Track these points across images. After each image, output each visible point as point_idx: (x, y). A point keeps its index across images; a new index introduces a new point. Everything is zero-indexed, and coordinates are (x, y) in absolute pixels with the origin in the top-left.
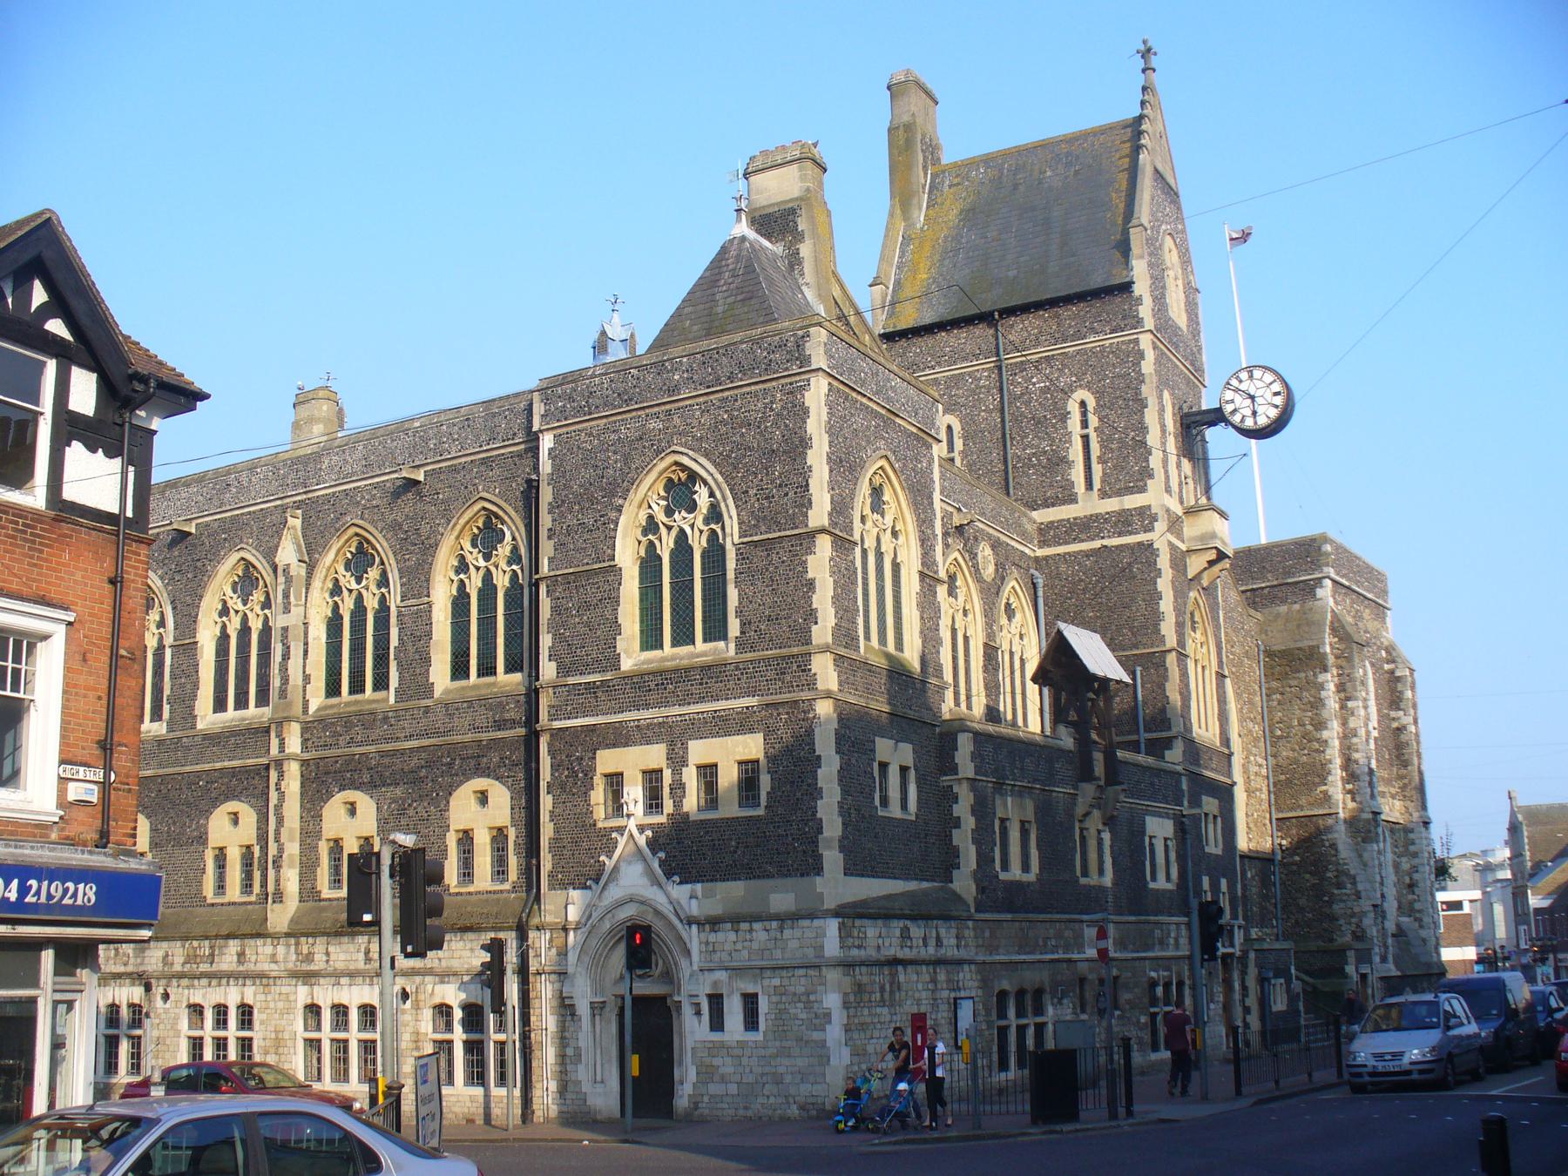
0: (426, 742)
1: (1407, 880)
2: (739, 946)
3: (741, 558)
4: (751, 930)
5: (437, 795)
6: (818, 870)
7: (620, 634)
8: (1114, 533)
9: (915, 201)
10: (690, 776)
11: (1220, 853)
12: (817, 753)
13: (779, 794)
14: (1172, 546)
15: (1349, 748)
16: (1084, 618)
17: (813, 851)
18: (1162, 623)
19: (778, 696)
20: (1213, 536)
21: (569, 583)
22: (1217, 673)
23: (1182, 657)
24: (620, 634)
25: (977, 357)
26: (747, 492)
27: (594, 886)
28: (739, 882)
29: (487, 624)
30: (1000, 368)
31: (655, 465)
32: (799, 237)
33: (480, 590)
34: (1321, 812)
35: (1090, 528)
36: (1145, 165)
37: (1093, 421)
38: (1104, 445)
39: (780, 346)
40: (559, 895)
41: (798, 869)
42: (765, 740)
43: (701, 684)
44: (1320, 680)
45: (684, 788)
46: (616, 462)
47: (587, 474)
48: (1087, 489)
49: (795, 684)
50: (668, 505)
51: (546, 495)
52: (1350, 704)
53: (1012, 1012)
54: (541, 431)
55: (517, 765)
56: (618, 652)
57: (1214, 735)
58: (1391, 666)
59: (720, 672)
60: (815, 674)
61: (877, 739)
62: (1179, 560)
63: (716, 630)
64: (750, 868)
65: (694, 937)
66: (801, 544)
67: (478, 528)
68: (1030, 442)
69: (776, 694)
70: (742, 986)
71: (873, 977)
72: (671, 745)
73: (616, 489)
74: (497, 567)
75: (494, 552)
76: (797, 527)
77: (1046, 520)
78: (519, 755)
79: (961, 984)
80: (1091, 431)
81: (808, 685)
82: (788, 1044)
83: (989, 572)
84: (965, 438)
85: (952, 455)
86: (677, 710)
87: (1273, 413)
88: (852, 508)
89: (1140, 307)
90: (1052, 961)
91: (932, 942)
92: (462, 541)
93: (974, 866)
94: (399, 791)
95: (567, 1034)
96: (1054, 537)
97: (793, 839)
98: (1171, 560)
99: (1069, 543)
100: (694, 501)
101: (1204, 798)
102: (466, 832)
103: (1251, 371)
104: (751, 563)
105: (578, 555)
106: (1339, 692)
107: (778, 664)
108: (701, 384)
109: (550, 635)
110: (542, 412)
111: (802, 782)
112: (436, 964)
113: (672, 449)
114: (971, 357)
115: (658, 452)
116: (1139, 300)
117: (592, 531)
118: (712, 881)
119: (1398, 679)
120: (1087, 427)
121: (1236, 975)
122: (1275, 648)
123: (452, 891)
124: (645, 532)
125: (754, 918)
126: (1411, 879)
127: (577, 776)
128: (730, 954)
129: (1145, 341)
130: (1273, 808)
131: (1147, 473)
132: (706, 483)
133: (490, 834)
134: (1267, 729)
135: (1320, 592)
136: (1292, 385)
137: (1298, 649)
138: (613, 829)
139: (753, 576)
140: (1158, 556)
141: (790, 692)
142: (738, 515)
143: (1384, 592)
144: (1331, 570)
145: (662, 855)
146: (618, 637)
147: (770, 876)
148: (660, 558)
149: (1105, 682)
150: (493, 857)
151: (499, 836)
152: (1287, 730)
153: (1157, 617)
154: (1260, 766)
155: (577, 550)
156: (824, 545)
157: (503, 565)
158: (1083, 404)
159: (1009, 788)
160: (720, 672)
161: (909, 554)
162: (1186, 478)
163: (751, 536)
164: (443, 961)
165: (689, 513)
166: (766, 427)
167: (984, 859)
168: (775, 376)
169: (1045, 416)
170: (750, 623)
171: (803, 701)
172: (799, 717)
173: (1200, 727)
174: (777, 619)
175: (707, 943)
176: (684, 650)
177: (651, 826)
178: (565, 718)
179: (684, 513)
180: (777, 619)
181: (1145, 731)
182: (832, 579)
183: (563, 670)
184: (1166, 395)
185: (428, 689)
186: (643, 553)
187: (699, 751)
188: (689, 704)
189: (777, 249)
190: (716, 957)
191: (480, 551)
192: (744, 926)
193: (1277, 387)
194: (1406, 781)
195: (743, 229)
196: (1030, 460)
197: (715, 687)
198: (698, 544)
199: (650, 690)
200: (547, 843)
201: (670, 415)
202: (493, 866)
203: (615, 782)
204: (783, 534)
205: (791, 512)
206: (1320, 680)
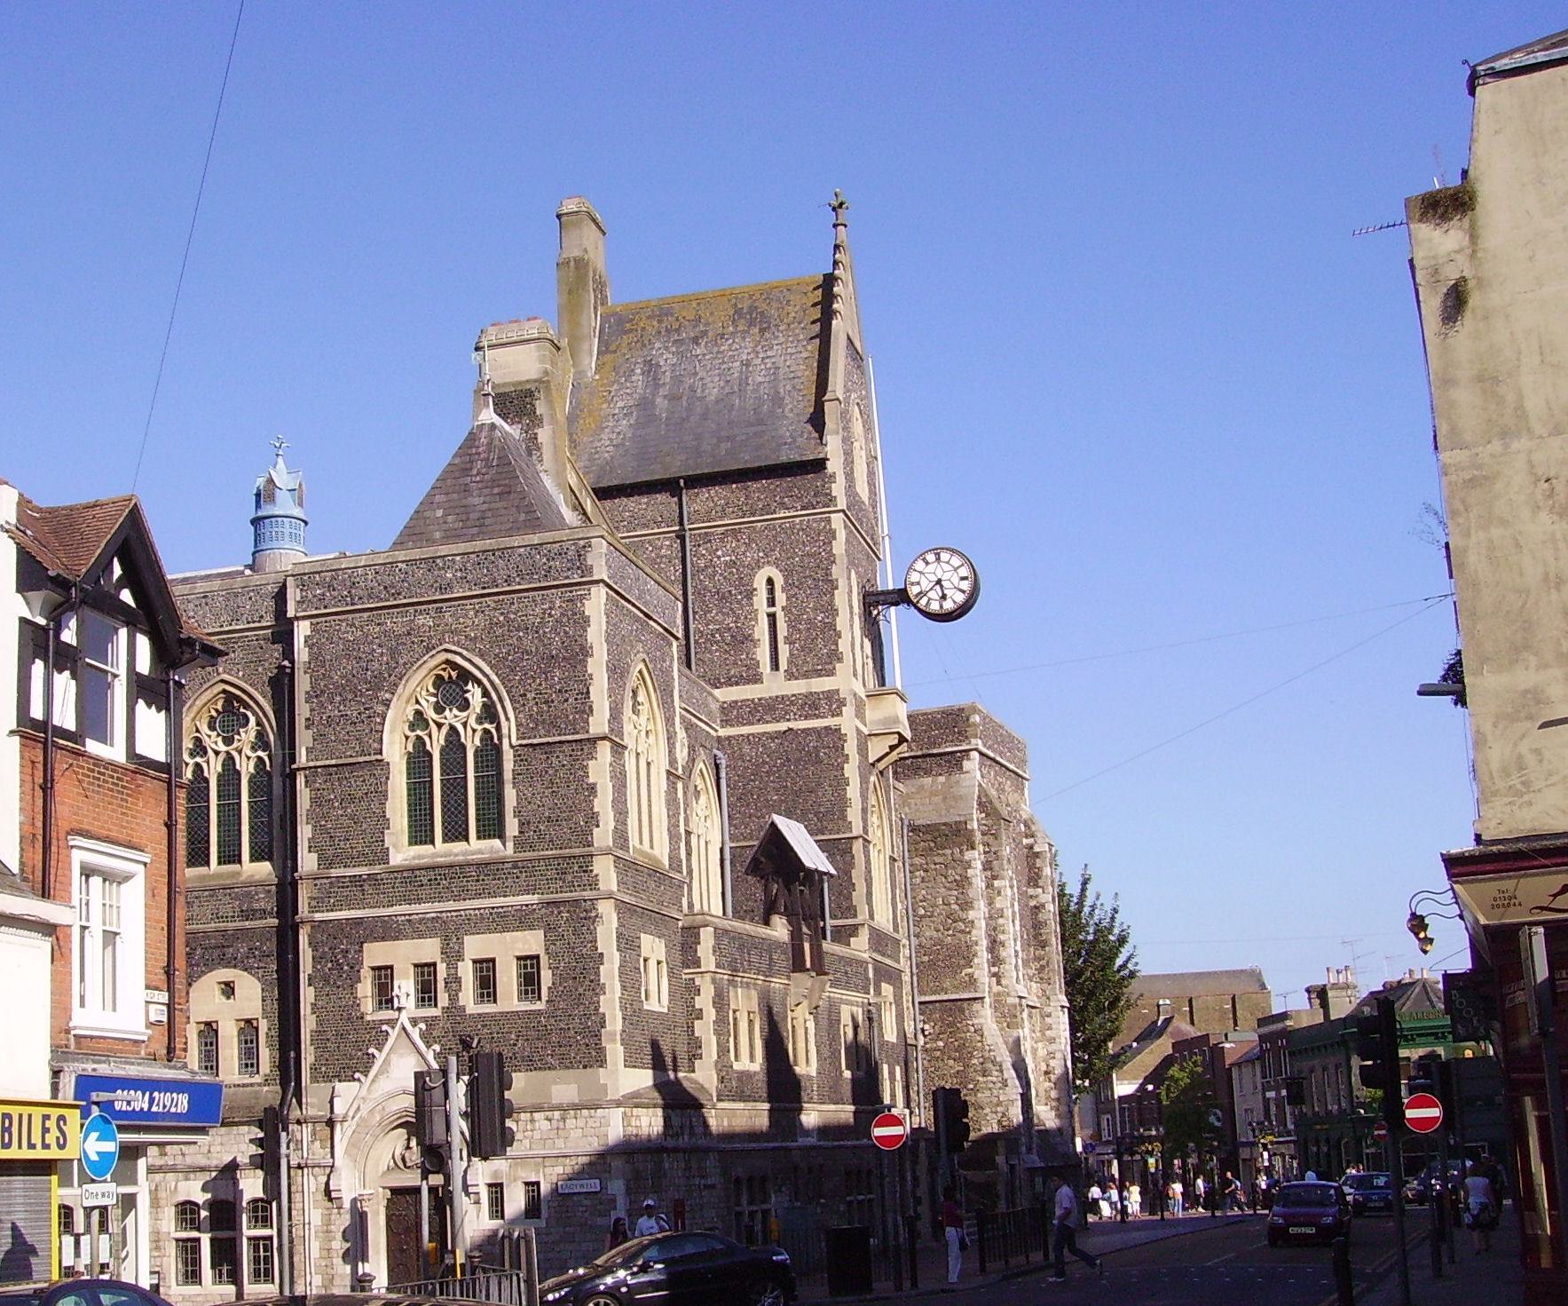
1: (1044, 1068)
4: (532, 1121)
6: (602, 1062)
7: (388, 828)
8: (800, 716)
9: (585, 346)
10: (466, 971)
12: (599, 951)
13: (561, 988)
14: (859, 731)
15: (995, 929)
16: (768, 801)
17: (596, 1044)
19: (560, 895)
21: (331, 774)
24: (388, 828)
26: (525, 695)
27: (363, 1078)
30: (682, 538)
32: (536, 421)
33: (219, 776)
34: (966, 996)
37: (781, 598)
39: (560, 554)
40: (324, 1088)
42: (545, 936)
43: (478, 881)
44: (966, 858)
45: (460, 982)
47: (349, 666)
48: (772, 669)
49: (576, 884)
50: (437, 702)
51: (303, 684)
52: (996, 883)
53: (744, 1201)
54: (297, 618)
55: (268, 956)
56: (386, 846)
58: (1030, 841)
59: (498, 870)
60: (597, 875)
63: (492, 827)
66: (582, 750)
67: (217, 710)
69: (557, 892)
70: (523, 1175)
72: (446, 939)
73: (381, 684)
74: (240, 752)
75: (236, 737)
76: (578, 733)
77: (729, 699)
78: (271, 946)
80: (778, 609)
81: (590, 885)
86: (451, 905)
87: (960, 598)
92: (198, 723)
93: (715, 1057)
97: (576, 1033)
99: (753, 724)
100: (466, 700)
101: (883, 984)
102: (208, 1024)
103: (939, 554)
104: (529, 765)
105: (341, 747)
106: (985, 870)
107: (559, 864)
108: (475, 585)
109: (310, 826)
110: (298, 599)
112: (179, 1160)
115: (428, 649)
119: (1037, 855)
121: (908, 1165)
122: (918, 823)
124: (412, 727)
125: (539, 1109)
126: (1048, 1066)
129: (837, 521)
130: (916, 991)
131: (836, 656)
132: (480, 683)
135: (966, 765)
136: (977, 570)
137: (945, 824)
138: (382, 1022)
139: (532, 778)
140: (845, 741)
141: (571, 891)
142: (516, 718)
143: (1023, 762)
144: (980, 742)
145: (437, 1047)
146: (386, 831)
148: (430, 755)
150: (240, 1049)
151: (248, 1027)
153: (843, 803)
157: (247, 751)
158: (770, 581)
159: (739, 979)
160: (498, 870)
161: (658, 754)
163: (529, 738)
164: (187, 1158)
165: (461, 711)
166: (544, 632)
167: (723, 1050)
168: (555, 583)
169: (730, 592)
170: (529, 823)
171: (585, 901)
172: (581, 915)
174: (557, 820)
176: (458, 847)
177: (425, 1019)
178: (328, 911)
179: (455, 711)
180: (557, 820)
183: (326, 861)
186: (410, 749)
187: (476, 946)
188: (465, 900)
189: (513, 431)
193: (964, 572)
194: (1042, 963)
195: (489, 415)
196: (713, 635)
198: (472, 743)
199: (422, 885)
201: (441, 612)
202: (240, 1059)
203: (384, 975)
204: (563, 738)
205: (571, 717)
206: (966, 858)
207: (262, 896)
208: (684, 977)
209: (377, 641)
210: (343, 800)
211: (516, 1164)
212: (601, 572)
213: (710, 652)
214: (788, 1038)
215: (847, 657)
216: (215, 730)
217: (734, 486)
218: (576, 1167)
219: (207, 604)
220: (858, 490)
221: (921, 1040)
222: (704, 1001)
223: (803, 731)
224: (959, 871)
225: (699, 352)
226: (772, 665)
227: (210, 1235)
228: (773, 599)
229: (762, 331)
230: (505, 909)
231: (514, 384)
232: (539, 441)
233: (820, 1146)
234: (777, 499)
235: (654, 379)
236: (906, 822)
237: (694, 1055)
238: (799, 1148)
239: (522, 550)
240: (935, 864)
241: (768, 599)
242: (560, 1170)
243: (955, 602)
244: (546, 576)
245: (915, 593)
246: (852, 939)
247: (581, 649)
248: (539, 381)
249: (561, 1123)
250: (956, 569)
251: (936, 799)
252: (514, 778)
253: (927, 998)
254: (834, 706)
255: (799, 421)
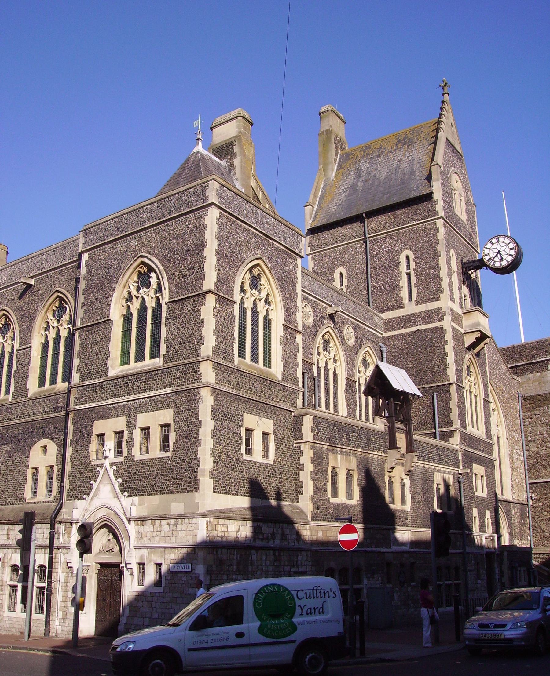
0: (23, 420)
2: (154, 534)
3: (169, 310)
5: (25, 449)
7: (109, 357)
8: (423, 323)
9: (330, 167)
10: (137, 434)
11: (486, 496)
14: (454, 328)
17: (195, 477)
18: (448, 369)
19: (182, 387)
20: (478, 324)
21: (89, 331)
22: (484, 400)
23: (460, 388)
24: (109, 357)
25: (354, 237)
26: (174, 274)
28: (156, 496)
29: (56, 355)
30: (365, 242)
31: (132, 264)
32: (234, 155)
35: (410, 320)
36: (441, 137)
37: (413, 265)
38: (418, 278)
41: (186, 489)
42: (174, 412)
43: (145, 382)
46: (115, 265)
47: (102, 272)
49: (191, 379)
50: (138, 286)
51: (82, 285)
56: (108, 366)
57: (482, 432)
60: (201, 373)
61: (244, 414)
62: (459, 337)
63: (155, 354)
64: (162, 488)
65: (133, 528)
66: (198, 300)
68: (380, 278)
71: (231, 556)
72: (129, 416)
76: (197, 291)
79: (299, 563)
81: (197, 380)
82: (175, 595)
83: (352, 341)
84: (349, 278)
85: (342, 287)
87: (510, 259)
88: (234, 283)
89: (436, 205)
90: (367, 552)
91: (278, 537)
92: (48, 314)
94: (9, 447)
95: (69, 584)
96: (392, 327)
97: (185, 470)
98: (453, 336)
103: (498, 238)
104: (173, 313)
110: (83, 242)
111: (191, 436)
113: (140, 254)
114: (352, 238)
116: (436, 202)
117: (101, 302)
118: (143, 495)
120: (409, 269)
121: (496, 565)
122: (526, 395)
123: (27, 501)
125: (162, 518)
127: (84, 436)
128: (150, 539)
129: (440, 223)
130: (527, 477)
132: (156, 272)
133: (46, 469)
134: (523, 437)
137: (540, 395)
140: (446, 333)
145: (120, 480)
147: (172, 493)
149: (403, 393)
150: (47, 482)
152: (534, 437)
153: (445, 366)
154: (519, 455)
155: (94, 313)
156: (211, 301)
158: (408, 257)
159: (339, 449)
162: (465, 296)
166: (186, 238)
167: (319, 490)
169: (388, 265)
170: (171, 346)
172: (192, 398)
173: (473, 427)
174: (184, 343)
175: (139, 532)
178: (81, 404)
179: (145, 289)
180: (184, 343)
181: (439, 427)
182: (215, 320)
183: (83, 378)
184: (452, 252)
185: (26, 391)
187: (142, 420)
188: (139, 393)
190: (143, 541)
191: (56, 319)
192: (157, 522)
193: (511, 245)
196: (380, 287)
197: (151, 383)
198: (151, 304)
200: (68, 474)
202: (47, 488)
205: (194, 283)
207: (62, 399)
208: (295, 445)
209: (113, 257)
210: (92, 343)
211: (152, 552)
212: (213, 198)
213: (379, 295)
214: (385, 487)
215: (447, 291)
216: (55, 317)
217: (389, 213)
218: (180, 555)
219: (54, 254)
220: (458, 211)
221: (531, 502)
222: (306, 459)
223: (424, 330)
224: (547, 418)
225: (380, 160)
226: (409, 299)
227: (21, 584)
228: (409, 266)
229: (409, 146)
230: (157, 397)
231: (225, 141)
232: (234, 165)
233: (413, 552)
234: (410, 216)
235: (359, 175)
236: (520, 395)
237: (299, 492)
238: (392, 552)
239: (177, 195)
240: (535, 415)
241: (407, 266)
242: (172, 556)
243: (507, 261)
244: (186, 207)
245: (487, 259)
246: (450, 438)
247: (202, 244)
248: (236, 136)
249: (175, 527)
250: (507, 245)
251: (535, 384)
252: (166, 322)
253: (533, 481)
254: (440, 316)
255: (421, 179)
